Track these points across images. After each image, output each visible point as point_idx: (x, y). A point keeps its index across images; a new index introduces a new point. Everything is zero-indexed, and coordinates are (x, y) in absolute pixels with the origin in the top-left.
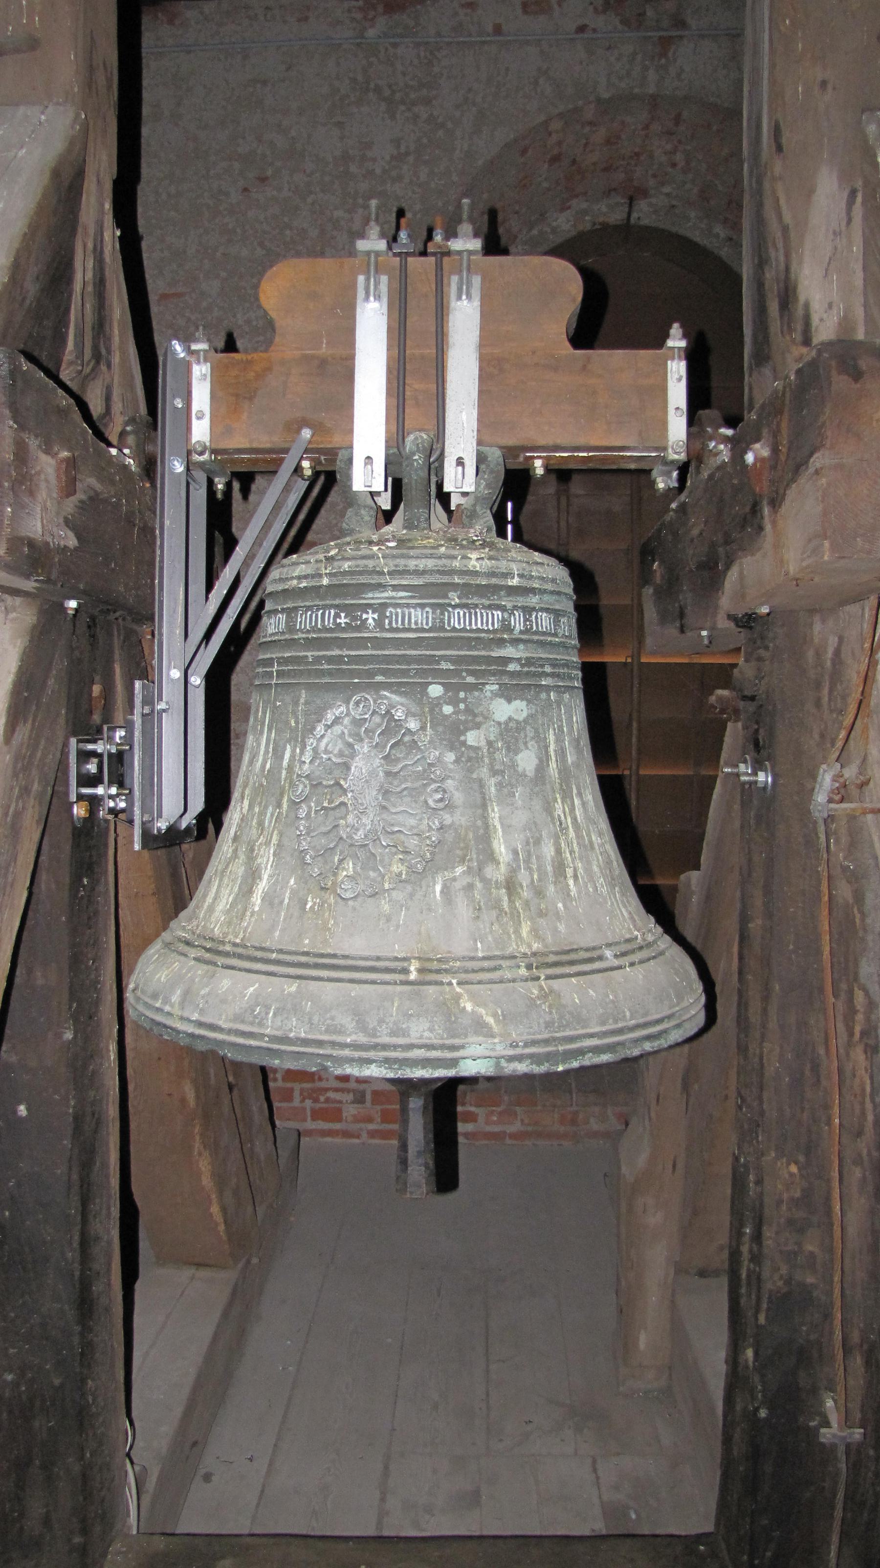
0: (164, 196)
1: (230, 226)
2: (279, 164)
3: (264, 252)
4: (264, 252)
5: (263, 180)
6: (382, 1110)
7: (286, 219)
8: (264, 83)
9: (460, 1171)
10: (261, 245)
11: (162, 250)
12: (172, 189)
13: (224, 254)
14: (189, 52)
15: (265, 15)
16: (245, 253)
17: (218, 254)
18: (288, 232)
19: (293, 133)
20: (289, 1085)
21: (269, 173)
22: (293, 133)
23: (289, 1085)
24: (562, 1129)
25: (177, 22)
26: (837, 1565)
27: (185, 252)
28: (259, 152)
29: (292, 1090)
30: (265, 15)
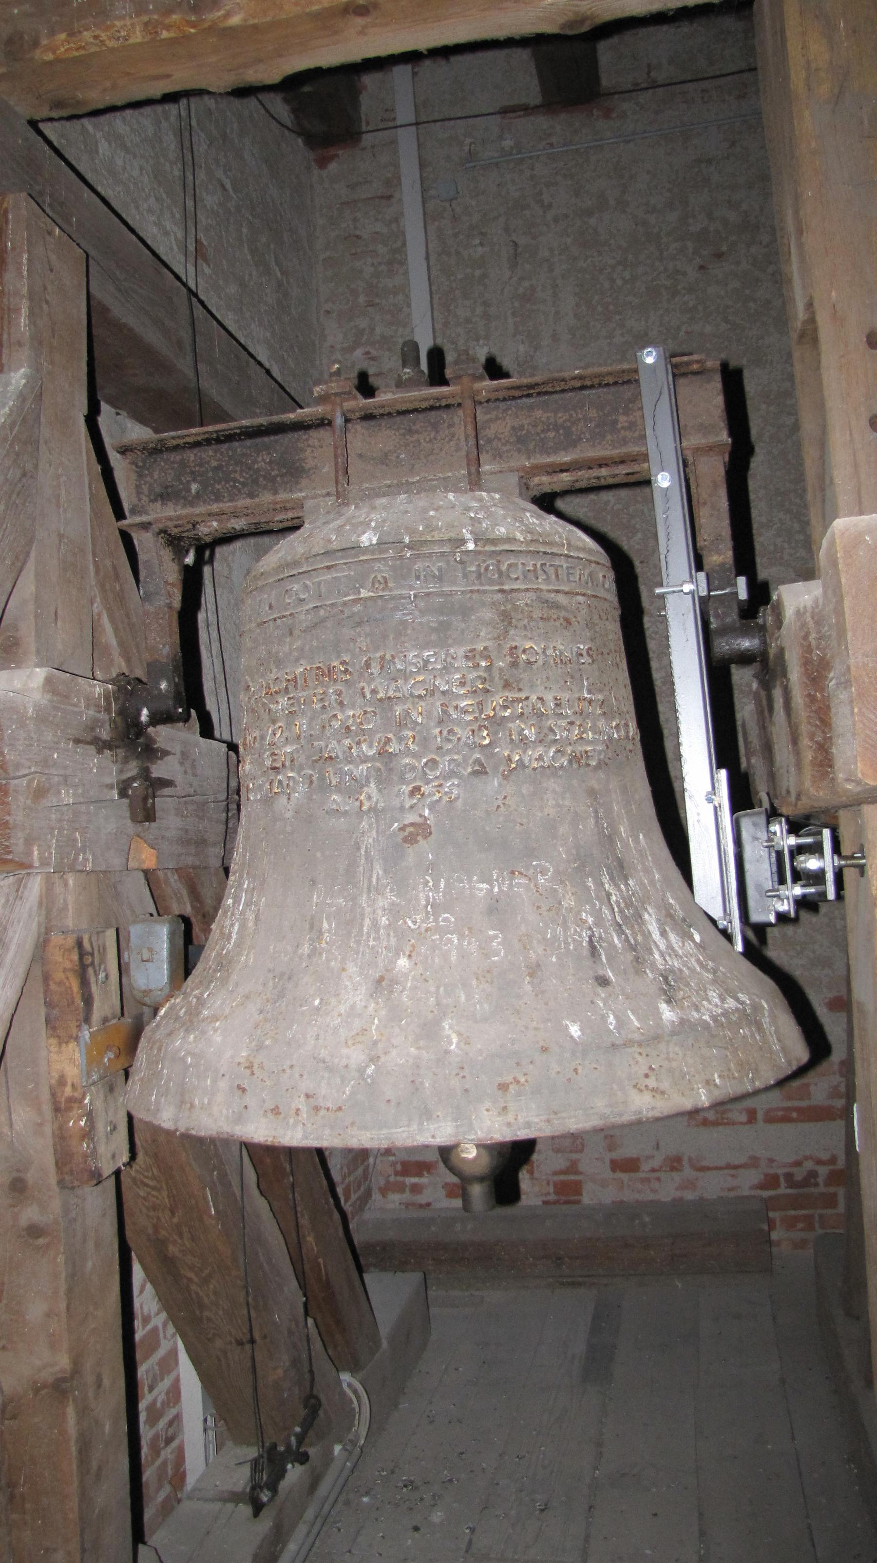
0: (619, 282)
1: (691, 304)
2: (734, 238)
3: (729, 326)
4: (729, 326)
5: (719, 256)
6: (809, 1099)
7: (747, 292)
8: (709, 161)
9: (117, 481)
10: (726, 320)
11: (622, 335)
12: (627, 275)
13: (687, 333)
14: (628, 142)
15: (703, 98)
16: (708, 329)
17: (682, 333)
18: (751, 304)
19: (744, 206)
20: (832, 1190)
21: (724, 248)
22: (744, 206)
23: (832, 1190)
24: (488, 417)
25: (614, 115)
26: (82, 1560)
27: (646, 334)
28: (712, 229)
29: (835, 1195)
30: (703, 98)
